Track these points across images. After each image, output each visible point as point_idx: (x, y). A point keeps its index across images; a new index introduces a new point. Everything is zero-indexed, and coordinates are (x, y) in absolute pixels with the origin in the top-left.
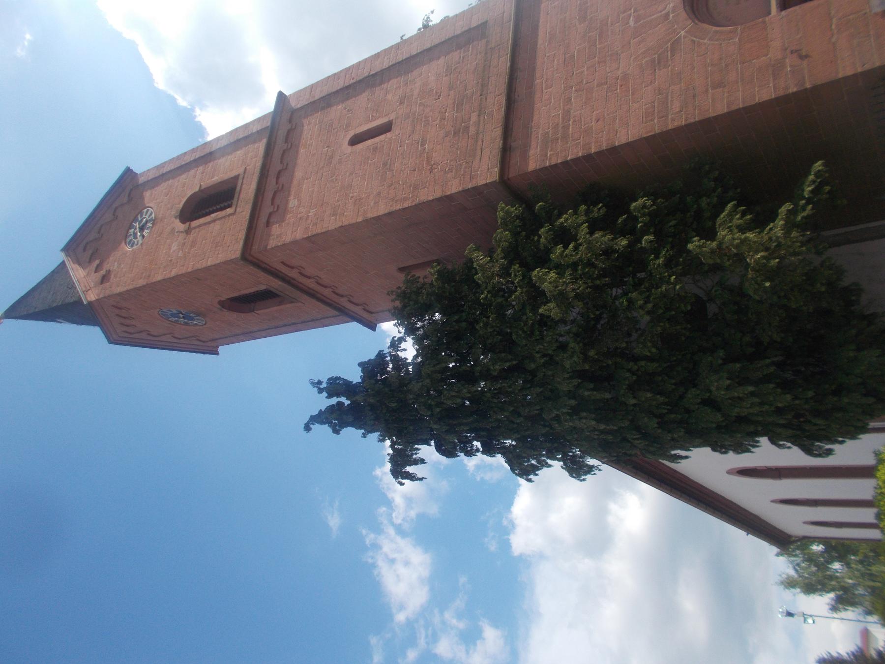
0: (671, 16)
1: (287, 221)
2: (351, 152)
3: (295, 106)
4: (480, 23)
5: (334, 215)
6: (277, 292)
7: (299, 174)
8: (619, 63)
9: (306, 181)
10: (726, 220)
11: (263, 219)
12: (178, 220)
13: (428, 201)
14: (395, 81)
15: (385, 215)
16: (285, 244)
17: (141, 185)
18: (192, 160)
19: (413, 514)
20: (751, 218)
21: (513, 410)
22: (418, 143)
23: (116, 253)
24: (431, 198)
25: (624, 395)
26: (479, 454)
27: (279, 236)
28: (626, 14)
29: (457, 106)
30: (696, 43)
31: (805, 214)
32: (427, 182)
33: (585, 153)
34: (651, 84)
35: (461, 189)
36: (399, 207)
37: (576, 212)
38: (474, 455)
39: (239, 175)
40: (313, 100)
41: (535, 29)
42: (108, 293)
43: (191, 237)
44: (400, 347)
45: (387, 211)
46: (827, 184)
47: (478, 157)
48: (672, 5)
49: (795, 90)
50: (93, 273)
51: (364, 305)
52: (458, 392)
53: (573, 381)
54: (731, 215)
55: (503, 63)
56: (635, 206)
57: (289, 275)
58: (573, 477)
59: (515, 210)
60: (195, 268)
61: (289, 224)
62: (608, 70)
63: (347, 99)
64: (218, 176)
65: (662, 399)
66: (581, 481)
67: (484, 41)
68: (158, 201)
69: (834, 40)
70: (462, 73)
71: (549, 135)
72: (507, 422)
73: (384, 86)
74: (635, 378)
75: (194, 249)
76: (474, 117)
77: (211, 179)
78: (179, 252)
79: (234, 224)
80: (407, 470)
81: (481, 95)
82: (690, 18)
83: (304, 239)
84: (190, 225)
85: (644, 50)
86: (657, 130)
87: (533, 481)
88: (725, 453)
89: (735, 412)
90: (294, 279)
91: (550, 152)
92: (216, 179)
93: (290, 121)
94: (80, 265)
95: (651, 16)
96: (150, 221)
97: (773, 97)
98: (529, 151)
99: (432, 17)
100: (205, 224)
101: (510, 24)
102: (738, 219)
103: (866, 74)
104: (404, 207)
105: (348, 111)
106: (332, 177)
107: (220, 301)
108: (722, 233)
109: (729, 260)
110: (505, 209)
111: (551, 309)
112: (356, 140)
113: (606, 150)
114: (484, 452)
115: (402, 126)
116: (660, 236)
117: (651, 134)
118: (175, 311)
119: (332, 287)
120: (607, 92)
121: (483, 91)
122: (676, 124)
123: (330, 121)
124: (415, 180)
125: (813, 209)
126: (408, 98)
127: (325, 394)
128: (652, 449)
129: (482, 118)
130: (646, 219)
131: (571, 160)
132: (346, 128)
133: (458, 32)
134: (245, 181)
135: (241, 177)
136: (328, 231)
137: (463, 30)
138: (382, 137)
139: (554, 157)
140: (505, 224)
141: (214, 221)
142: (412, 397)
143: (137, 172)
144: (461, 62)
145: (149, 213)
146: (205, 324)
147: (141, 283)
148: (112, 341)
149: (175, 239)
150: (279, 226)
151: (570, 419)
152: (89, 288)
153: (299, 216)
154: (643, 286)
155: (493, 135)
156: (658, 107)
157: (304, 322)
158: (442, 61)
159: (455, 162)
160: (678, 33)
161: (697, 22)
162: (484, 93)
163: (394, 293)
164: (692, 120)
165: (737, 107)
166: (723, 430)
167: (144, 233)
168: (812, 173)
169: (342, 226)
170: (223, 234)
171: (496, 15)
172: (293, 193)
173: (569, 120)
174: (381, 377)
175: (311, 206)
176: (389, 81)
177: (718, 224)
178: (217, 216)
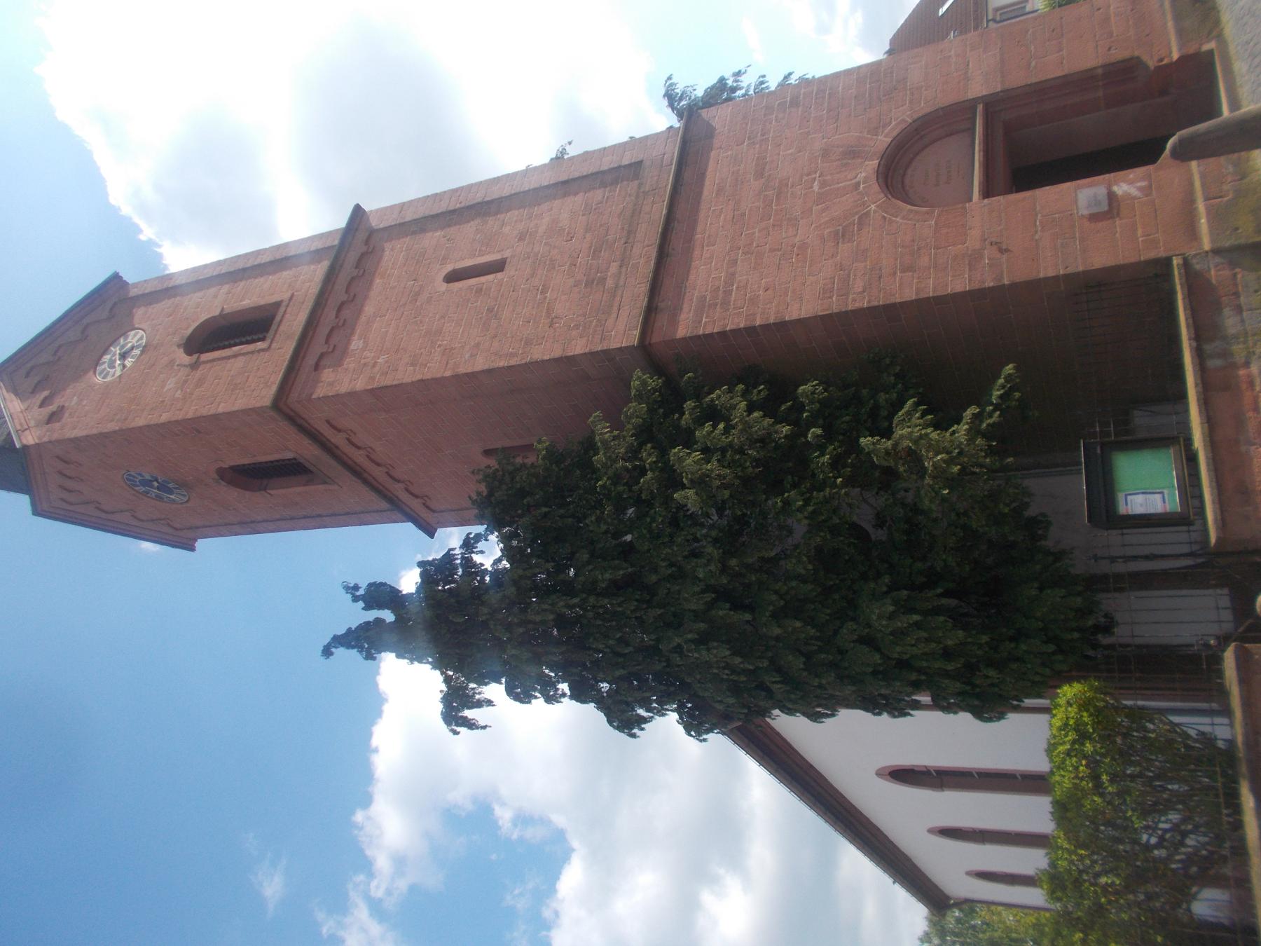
0: (862, 186)
1: (345, 366)
2: (446, 290)
3: (376, 226)
4: (633, 161)
5: (412, 365)
6: (307, 465)
7: (369, 309)
8: (798, 229)
9: (378, 319)
10: (904, 419)
11: (311, 360)
12: (182, 350)
13: (543, 361)
14: (516, 212)
15: (483, 371)
16: (338, 395)
17: (132, 298)
18: (214, 274)
19: (403, 884)
20: (932, 418)
21: (620, 638)
22: (538, 290)
23: (78, 384)
24: (546, 358)
25: (765, 624)
26: (566, 700)
27: (331, 384)
28: (810, 177)
29: (594, 252)
30: (887, 219)
31: (990, 421)
32: (544, 337)
33: (749, 324)
34: (832, 258)
35: (587, 350)
36: (502, 363)
37: (730, 391)
38: (558, 702)
39: (282, 301)
40: (402, 221)
41: (702, 176)
42: (56, 436)
43: (198, 373)
44: (477, 547)
45: (486, 367)
46: (1017, 390)
47: (614, 315)
48: (863, 175)
49: (992, 284)
50: (36, 408)
51: (425, 498)
52: (552, 605)
53: (705, 595)
54: (909, 415)
55: (659, 211)
56: (804, 390)
57: (332, 440)
58: (691, 736)
59: (653, 382)
60: (199, 414)
61: (347, 369)
62: (784, 235)
63: (450, 226)
64: (250, 300)
65: (813, 631)
66: (701, 741)
67: (636, 182)
68: (154, 322)
69: (1037, 237)
70: (604, 215)
71: (705, 299)
72: (610, 655)
73: (501, 216)
74: (782, 603)
75: (201, 389)
76: (614, 267)
77: (241, 301)
78: (176, 391)
79: (265, 363)
80: (465, 715)
81: (626, 243)
82: (883, 192)
83: (367, 390)
84: (198, 358)
85: (827, 219)
86: (835, 309)
87: (638, 737)
88: (879, 714)
89: (896, 652)
90: (337, 447)
91: (705, 318)
92: (247, 303)
93: (367, 242)
94: (16, 394)
95: (838, 183)
96: (138, 347)
97: (967, 289)
98: (680, 316)
99: (568, 148)
100: (223, 358)
101: (671, 169)
102: (918, 418)
103: (1068, 278)
104: (510, 365)
105: (448, 240)
106: (416, 318)
107: (221, 468)
108: (899, 432)
109: (903, 464)
110: (640, 379)
111: (688, 497)
112: (453, 277)
113: (774, 324)
114: (572, 697)
115: (519, 267)
116: (829, 434)
117: (827, 312)
118: (148, 477)
119: (388, 466)
120: (780, 259)
121: (628, 239)
122: (857, 305)
123: (422, 248)
124: (529, 334)
125: (1000, 416)
126: (530, 235)
127: (361, 604)
128: (793, 696)
129: (624, 269)
130: (816, 406)
131: (731, 331)
132: (443, 259)
133: (605, 168)
134: (289, 310)
135: (284, 304)
136: (402, 384)
137: (612, 166)
138: (490, 277)
139: (711, 324)
140: (640, 397)
141: (235, 356)
142: (486, 612)
143: (128, 281)
144: (604, 202)
145: (138, 337)
146: (187, 501)
147: (112, 426)
148: (37, 511)
149: (173, 374)
150: (332, 371)
151: (695, 649)
152: (26, 427)
153: (363, 361)
154: (803, 486)
155: (638, 290)
156: (838, 284)
157: (336, 515)
158: (579, 198)
159: (584, 318)
160: (868, 207)
161: (890, 197)
162: (629, 241)
163: (481, 472)
164: (876, 304)
165: (926, 296)
166: (880, 677)
167: (126, 362)
168: (1002, 377)
169: (422, 380)
170: (246, 374)
171: (654, 155)
172: (358, 332)
173: (733, 285)
174: (443, 587)
175: (381, 351)
176: (508, 211)
177: (895, 422)
178: (241, 349)
